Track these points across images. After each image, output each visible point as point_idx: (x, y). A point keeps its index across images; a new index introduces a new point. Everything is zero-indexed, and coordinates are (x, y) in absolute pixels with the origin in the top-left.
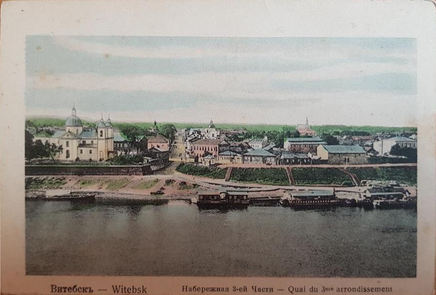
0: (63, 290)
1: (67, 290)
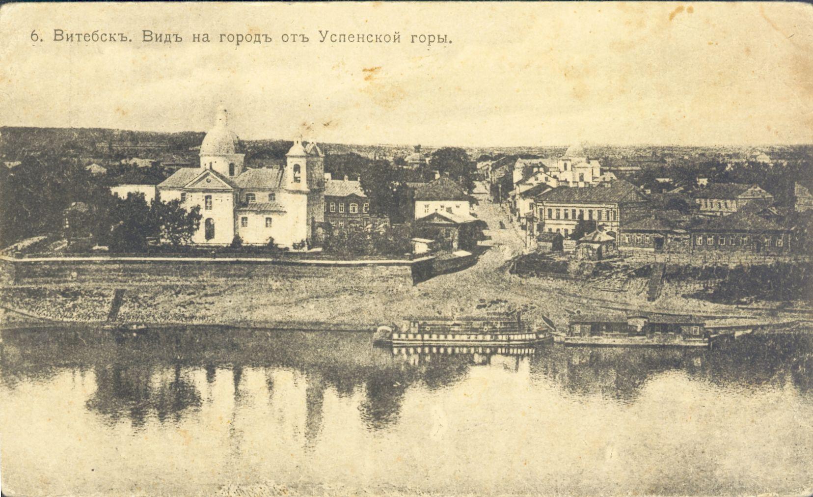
0: (75, 38)
1: (82, 38)
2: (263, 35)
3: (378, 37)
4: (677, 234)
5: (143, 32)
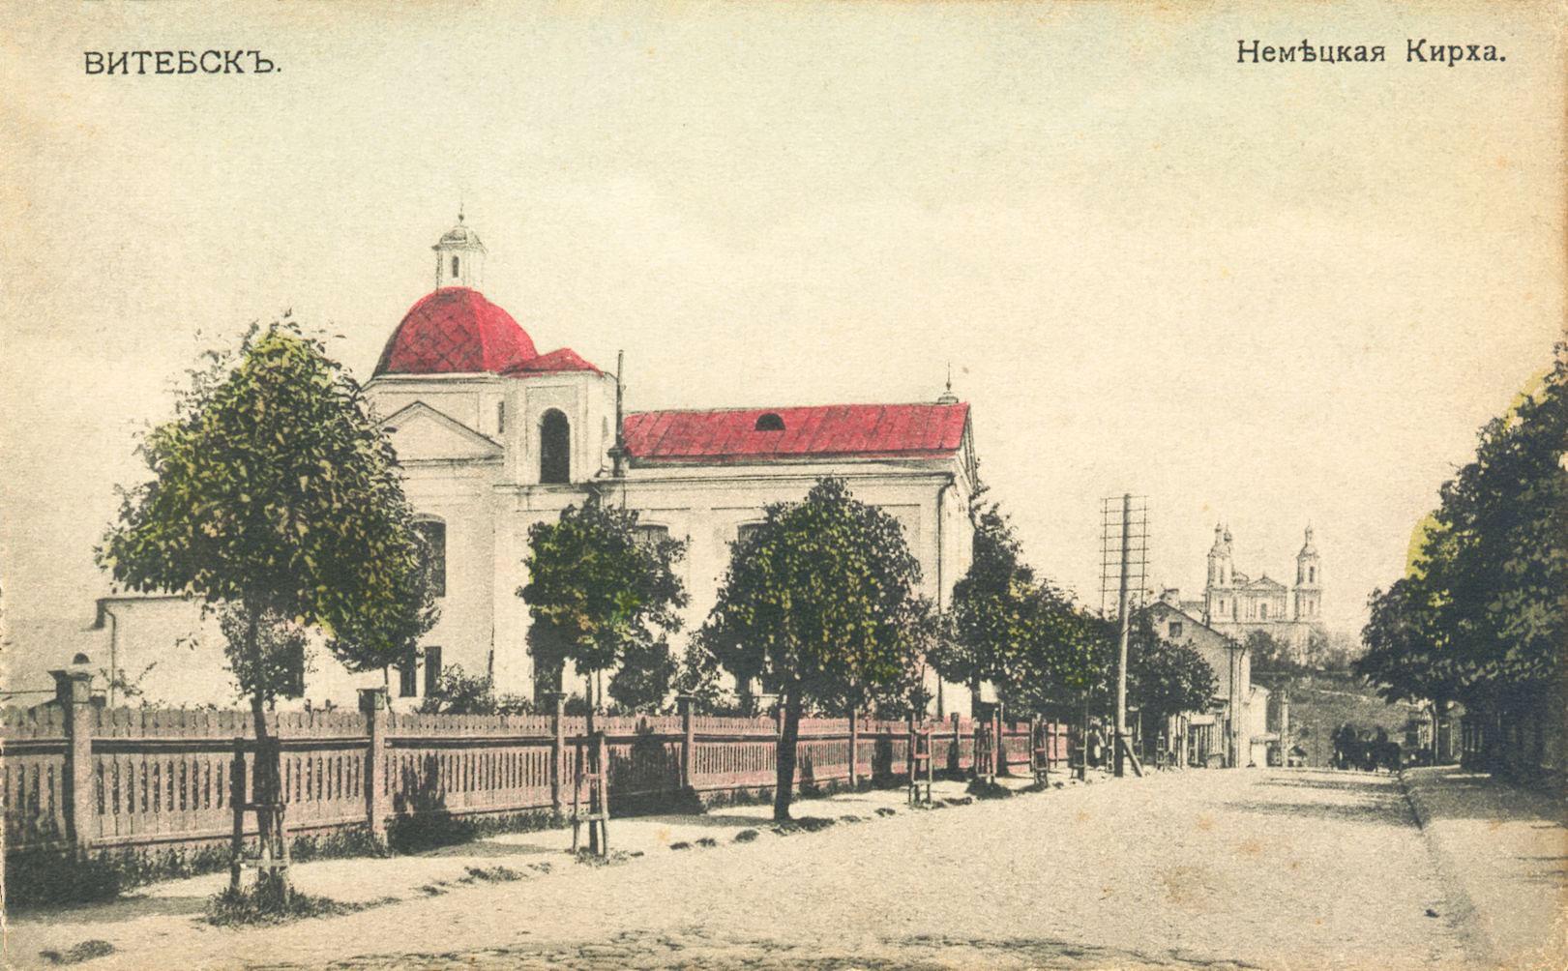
0: (133, 63)
1: (150, 63)
2: (133, 54)
3: (1414, 45)
4: (1477, 734)
5: (1238, 45)
